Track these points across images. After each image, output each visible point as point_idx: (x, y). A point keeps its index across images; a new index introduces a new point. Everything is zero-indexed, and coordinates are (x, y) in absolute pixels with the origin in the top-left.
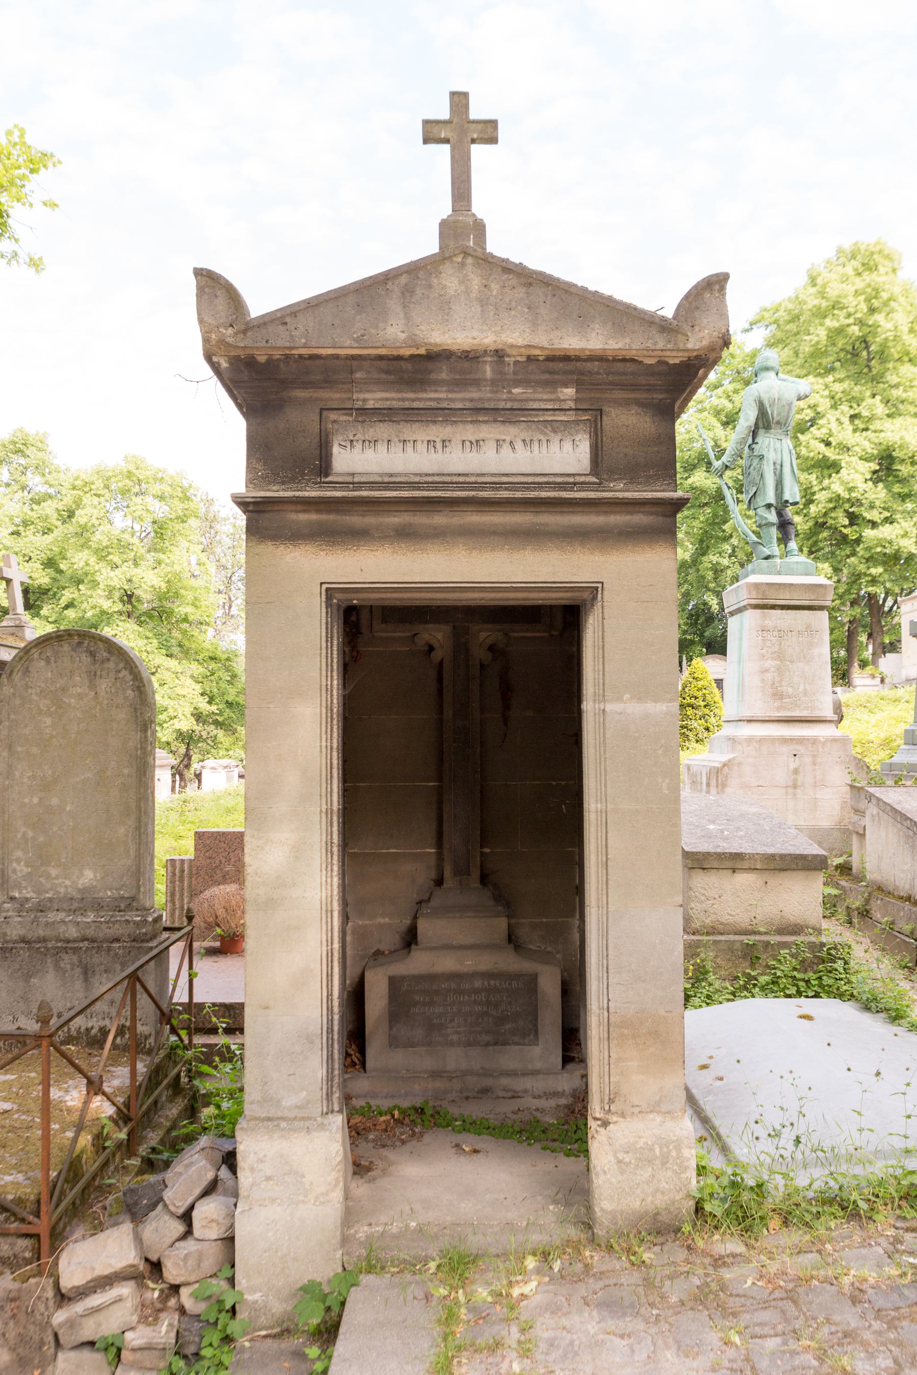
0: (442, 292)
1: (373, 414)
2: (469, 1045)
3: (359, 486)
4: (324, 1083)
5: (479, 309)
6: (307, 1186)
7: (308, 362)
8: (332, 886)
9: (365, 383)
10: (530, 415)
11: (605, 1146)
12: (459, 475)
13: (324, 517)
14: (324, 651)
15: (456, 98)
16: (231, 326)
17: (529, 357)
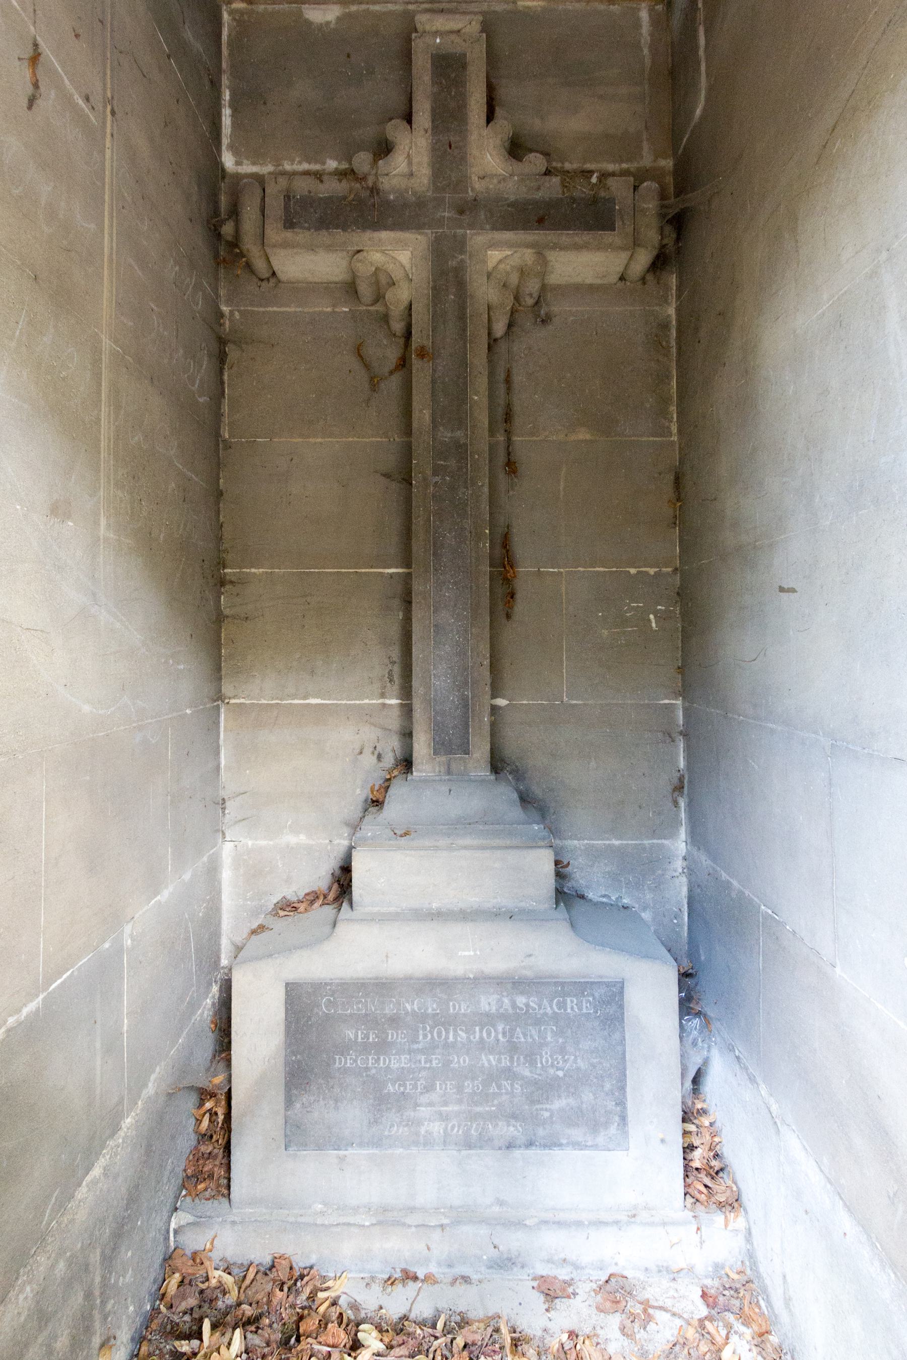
2: (469, 1146)
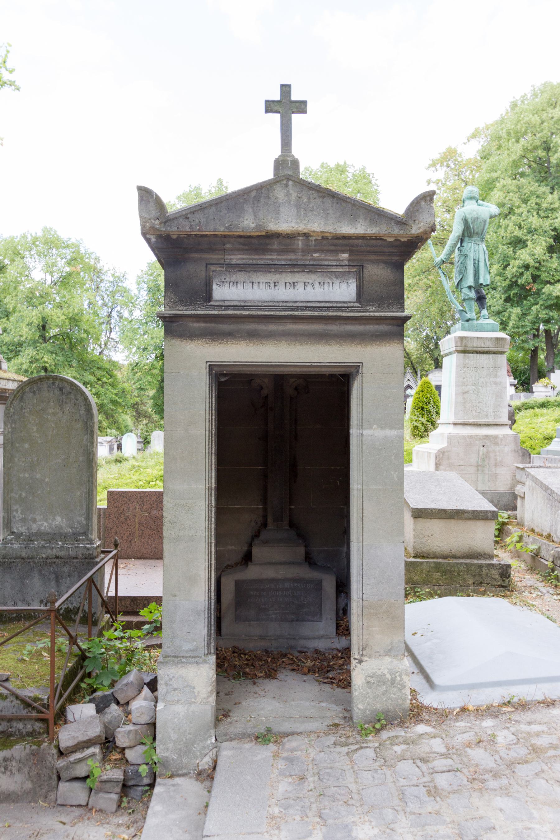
0: (276, 201)
1: (235, 267)
3: (227, 308)
4: (206, 637)
5: (296, 211)
6: (196, 694)
7: (200, 239)
8: (211, 529)
9: (231, 250)
10: (323, 268)
11: (359, 675)
12: (283, 302)
13: (208, 325)
14: (208, 400)
15: (284, 88)
16: (157, 219)
17: (323, 237)
